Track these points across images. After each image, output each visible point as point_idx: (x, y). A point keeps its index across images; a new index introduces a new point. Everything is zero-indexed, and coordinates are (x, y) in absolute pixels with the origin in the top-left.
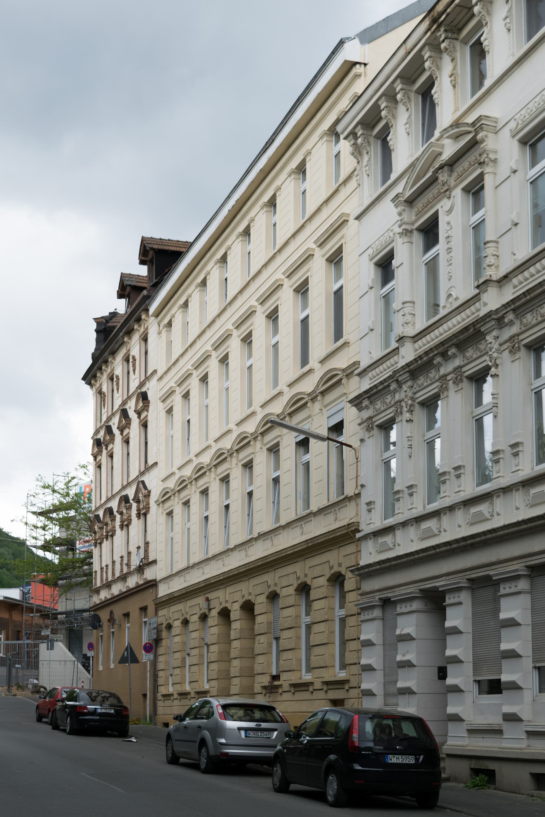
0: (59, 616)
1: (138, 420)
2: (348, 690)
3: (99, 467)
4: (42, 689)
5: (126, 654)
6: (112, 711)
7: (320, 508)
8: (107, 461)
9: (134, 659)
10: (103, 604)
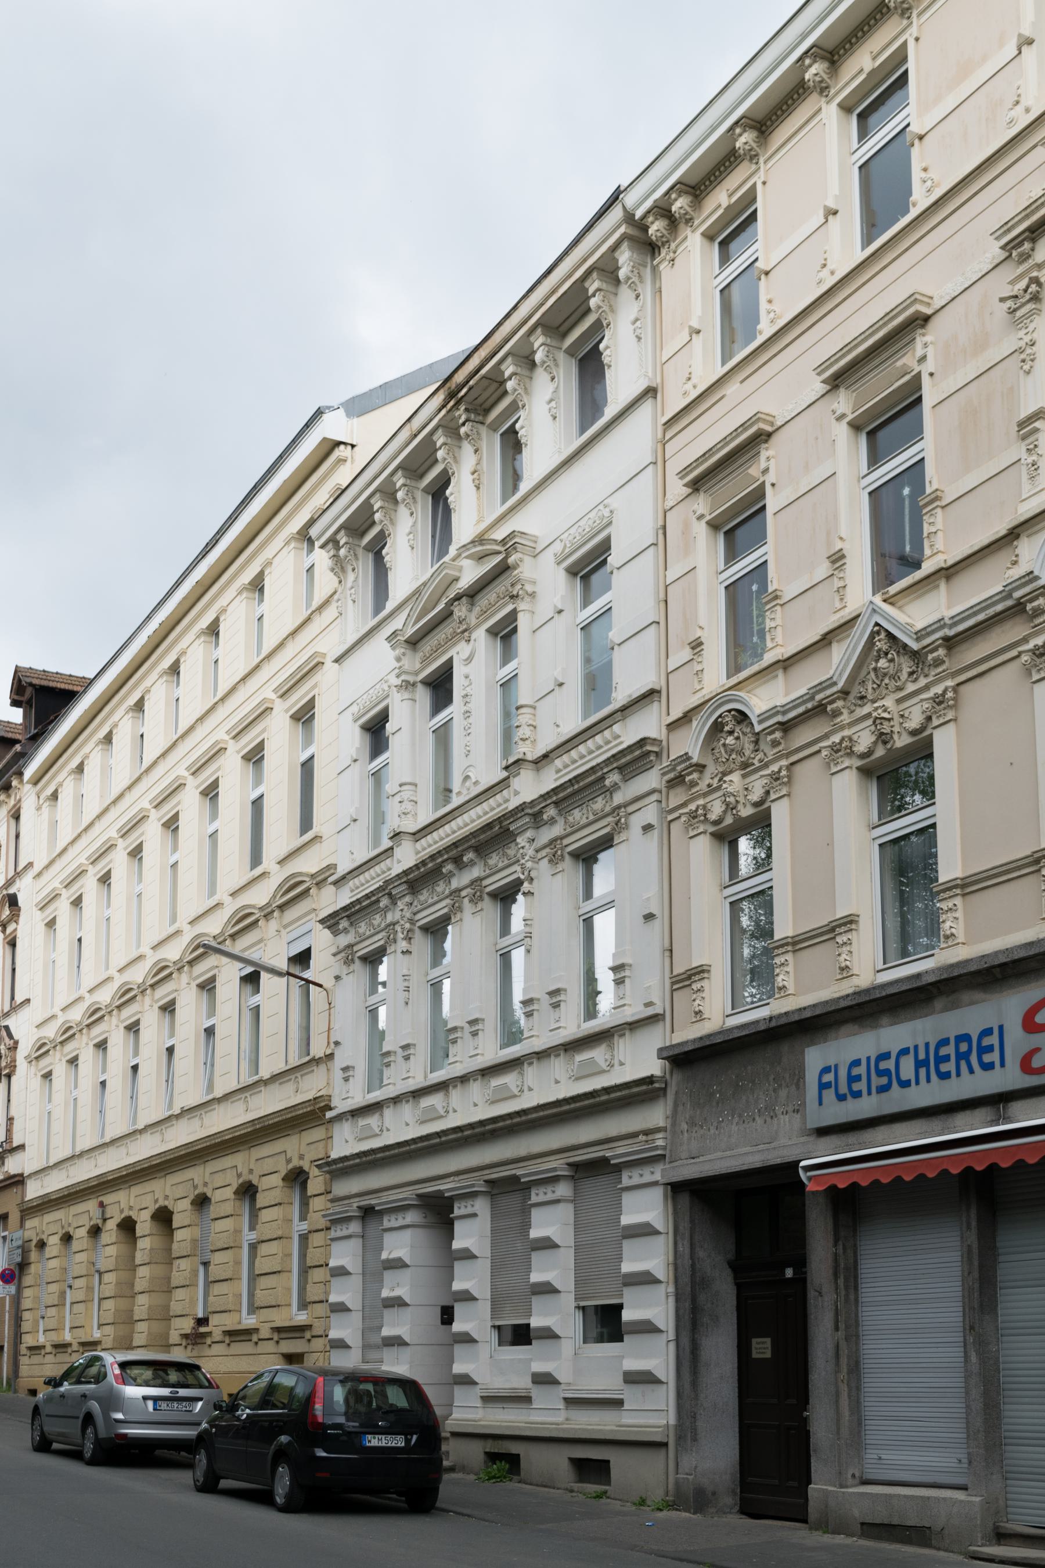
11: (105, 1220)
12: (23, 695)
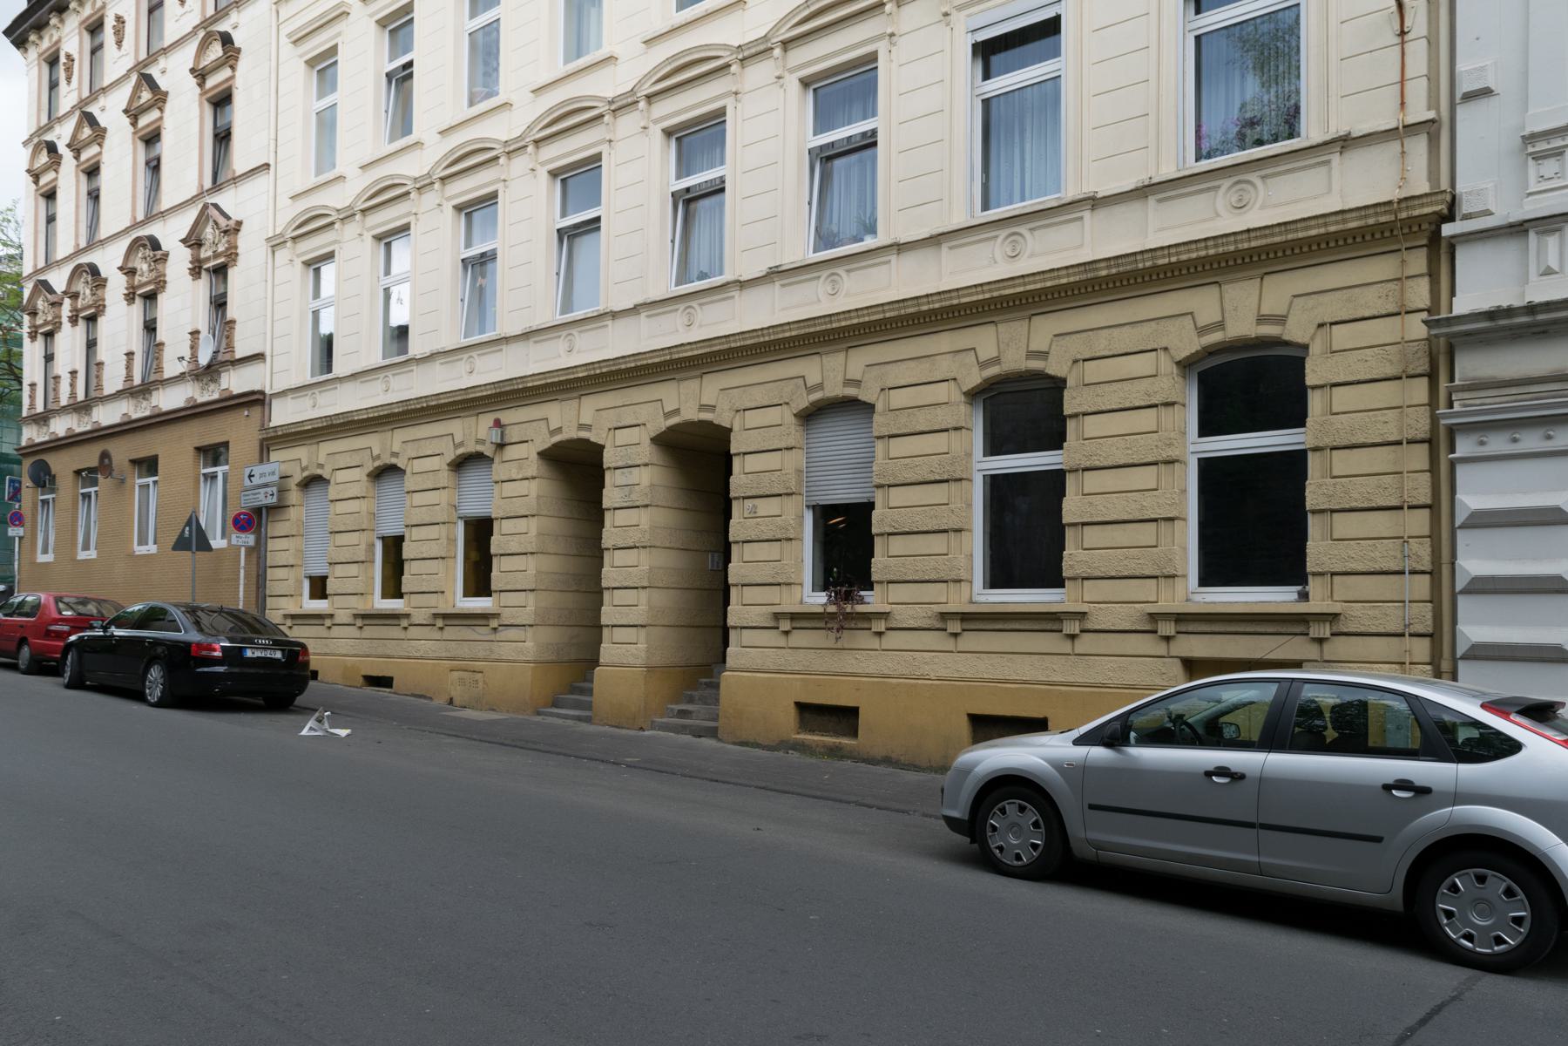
6: (278, 655)
7: (1154, 181)
8: (78, 181)
9: (203, 544)
11: (501, 446)
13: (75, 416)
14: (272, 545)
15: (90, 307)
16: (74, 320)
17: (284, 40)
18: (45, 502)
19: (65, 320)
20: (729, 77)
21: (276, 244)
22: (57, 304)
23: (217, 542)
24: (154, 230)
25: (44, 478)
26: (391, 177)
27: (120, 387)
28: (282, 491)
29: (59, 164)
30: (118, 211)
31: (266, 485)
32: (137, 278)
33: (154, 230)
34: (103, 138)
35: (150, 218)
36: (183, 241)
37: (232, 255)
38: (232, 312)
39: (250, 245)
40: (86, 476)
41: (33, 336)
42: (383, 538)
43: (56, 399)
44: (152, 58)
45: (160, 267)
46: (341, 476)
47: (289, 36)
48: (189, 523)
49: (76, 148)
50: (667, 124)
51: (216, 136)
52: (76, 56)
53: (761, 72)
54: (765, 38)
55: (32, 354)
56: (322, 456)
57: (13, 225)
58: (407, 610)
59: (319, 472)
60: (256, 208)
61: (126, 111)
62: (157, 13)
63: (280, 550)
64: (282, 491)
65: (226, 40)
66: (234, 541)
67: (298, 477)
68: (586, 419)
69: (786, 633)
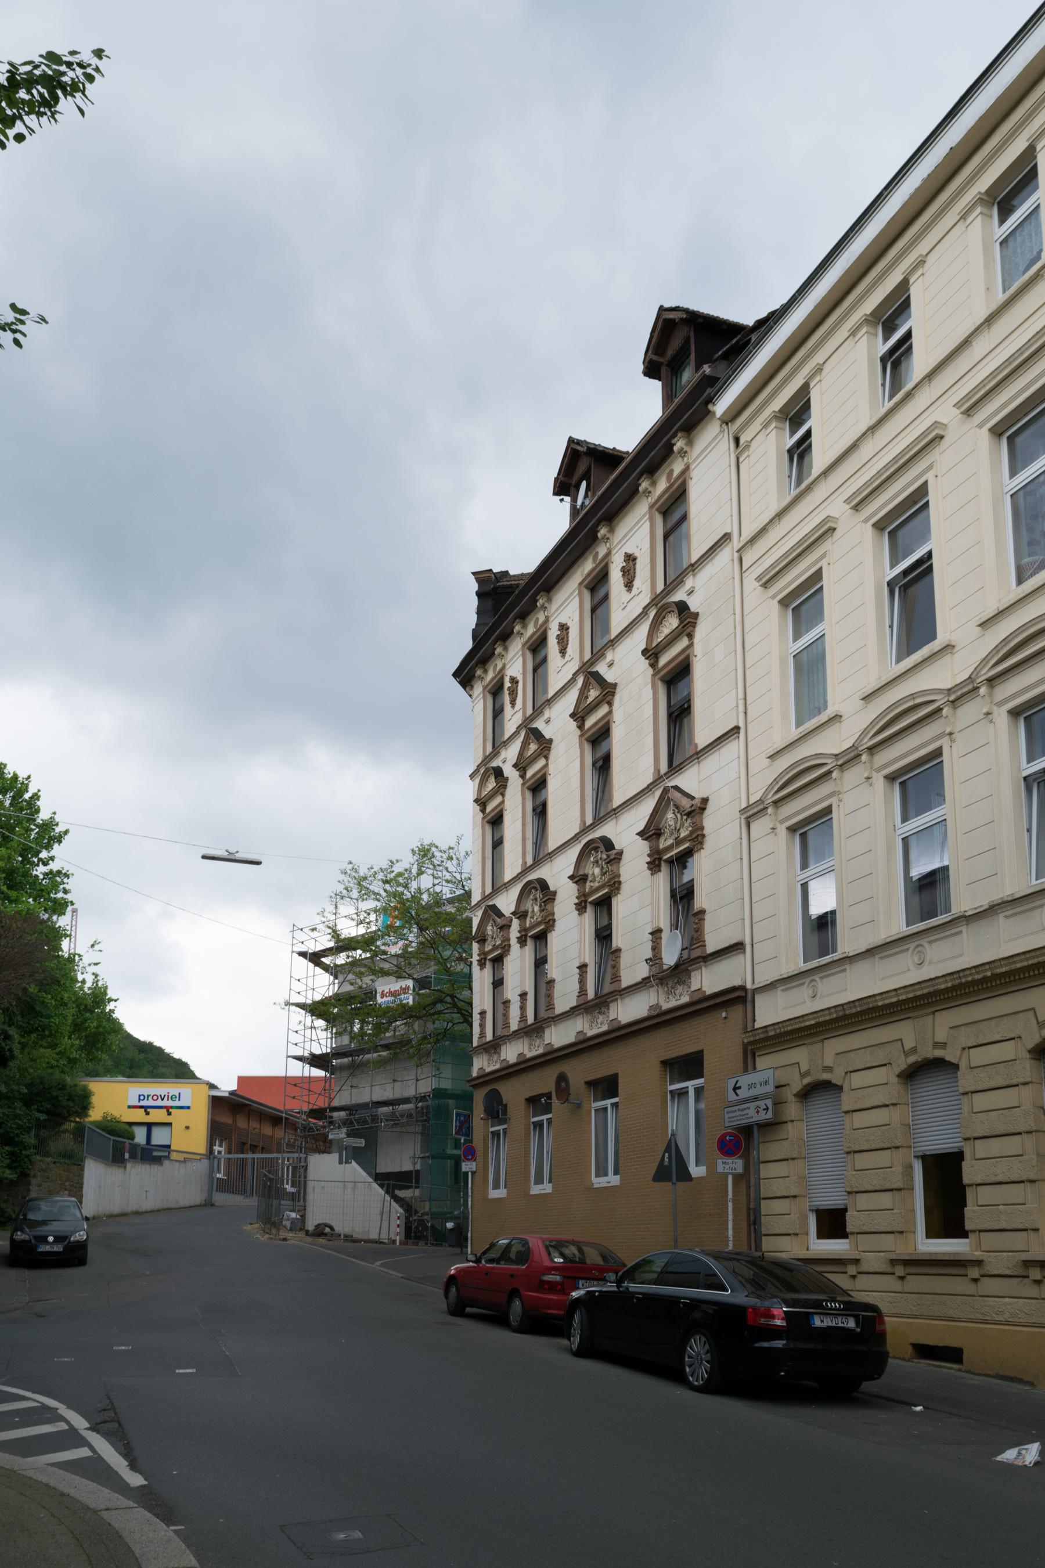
0: (335, 1114)
1: (521, 781)
2: (854, 1277)
3: (496, 821)
4: (327, 1230)
5: (666, 1160)
8: (524, 799)
9: (684, 1175)
10: (664, 1018)
12: (572, 477)
13: (526, 1041)
14: (766, 1171)
15: (538, 924)
16: (522, 941)
17: (751, 583)
18: (496, 1134)
19: (513, 941)
20: (942, 720)
21: (751, 814)
22: (506, 927)
23: (697, 1171)
24: (607, 830)
25: (496, 1110)
26: (913, 696)
27: (574, 1004)
28: (778, 1103)
29: (505, 787)
30: (566, 817)
31: (756, 1098)
32: (588, 884)
33: (607, 830)
34: (549, 749)
35: (599, 820)
36: (640, 834)
37: (697, 839)
38: (700, 901)
39: (721, 826)
40: (537, 1103)
41: (482, 964)
42: (925, 1158)
43: (506, 1025)
44: (597, 655)
45: (614, 867)
46: (858, 1080)
47: (758, 579)
48: (668, 1149)
49: (521, 766)
50: (1011, 705)
51: (670, 715)
52: (520, 678)
53: (855, 775)
54: (761, 801)
55: (481, 979)
56: (829, 1055)
57: (455, 862)
58: (978, 1254)
59: (826, 1076)
60: (719, 781)
61: (572, 715)
62: (540, 671)
63: (776, 1176)
64: (778, 1103)
65: (682, 608)
66: (720, 1168)
67: (797, 1085)
68: (941, 1036)
69: (902, 1278)
